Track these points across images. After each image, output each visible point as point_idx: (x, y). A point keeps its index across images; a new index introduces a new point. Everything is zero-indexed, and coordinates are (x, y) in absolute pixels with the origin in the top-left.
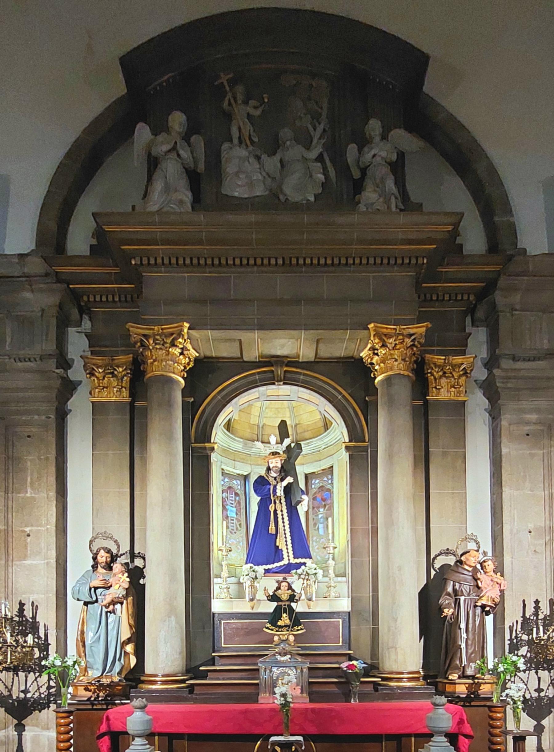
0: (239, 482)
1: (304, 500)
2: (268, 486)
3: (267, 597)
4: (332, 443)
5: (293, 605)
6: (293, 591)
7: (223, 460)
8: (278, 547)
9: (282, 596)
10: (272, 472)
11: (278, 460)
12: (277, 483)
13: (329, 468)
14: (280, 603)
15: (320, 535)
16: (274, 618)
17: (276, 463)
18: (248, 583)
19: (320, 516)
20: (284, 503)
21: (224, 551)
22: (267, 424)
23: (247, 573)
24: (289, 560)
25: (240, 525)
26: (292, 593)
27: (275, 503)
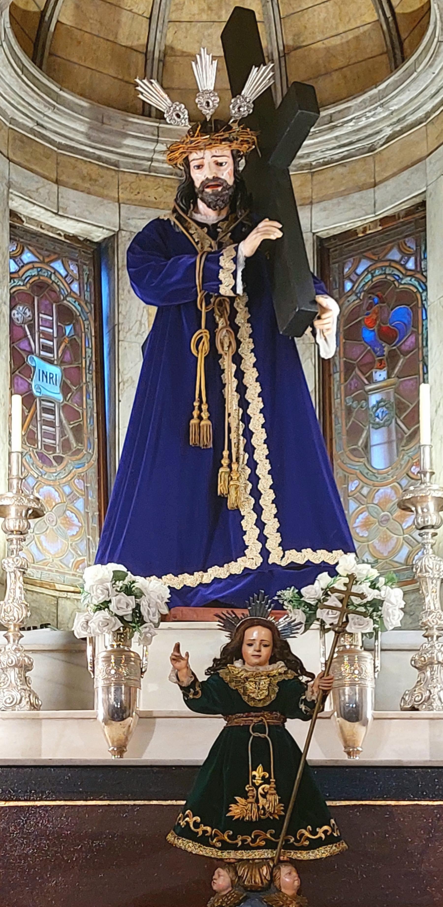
0: (74, 269)
1: (324, 310)
2: (186, 259)
3: (185, 690)
4: (420, 114)
5: (296, 728)
6: (296, 665)
7: (14, 177)
8: (224, 499)
9: (250, 686)
10: (201, 205)
11: (224, 153)
12: (221, 246)
13: (409, 212)
14: (240, 720)
15: (376, 473)
16: (210, 787)
17: (214, 165)
18: (105, 643)
19: (374, 399)
20: (245, 330)
21: (12, 512)
22: (178, 47)
23: (102, 598)
24: (265, 553)
25: (78, 431)
26: (290, 675)
27: (212, 326)
